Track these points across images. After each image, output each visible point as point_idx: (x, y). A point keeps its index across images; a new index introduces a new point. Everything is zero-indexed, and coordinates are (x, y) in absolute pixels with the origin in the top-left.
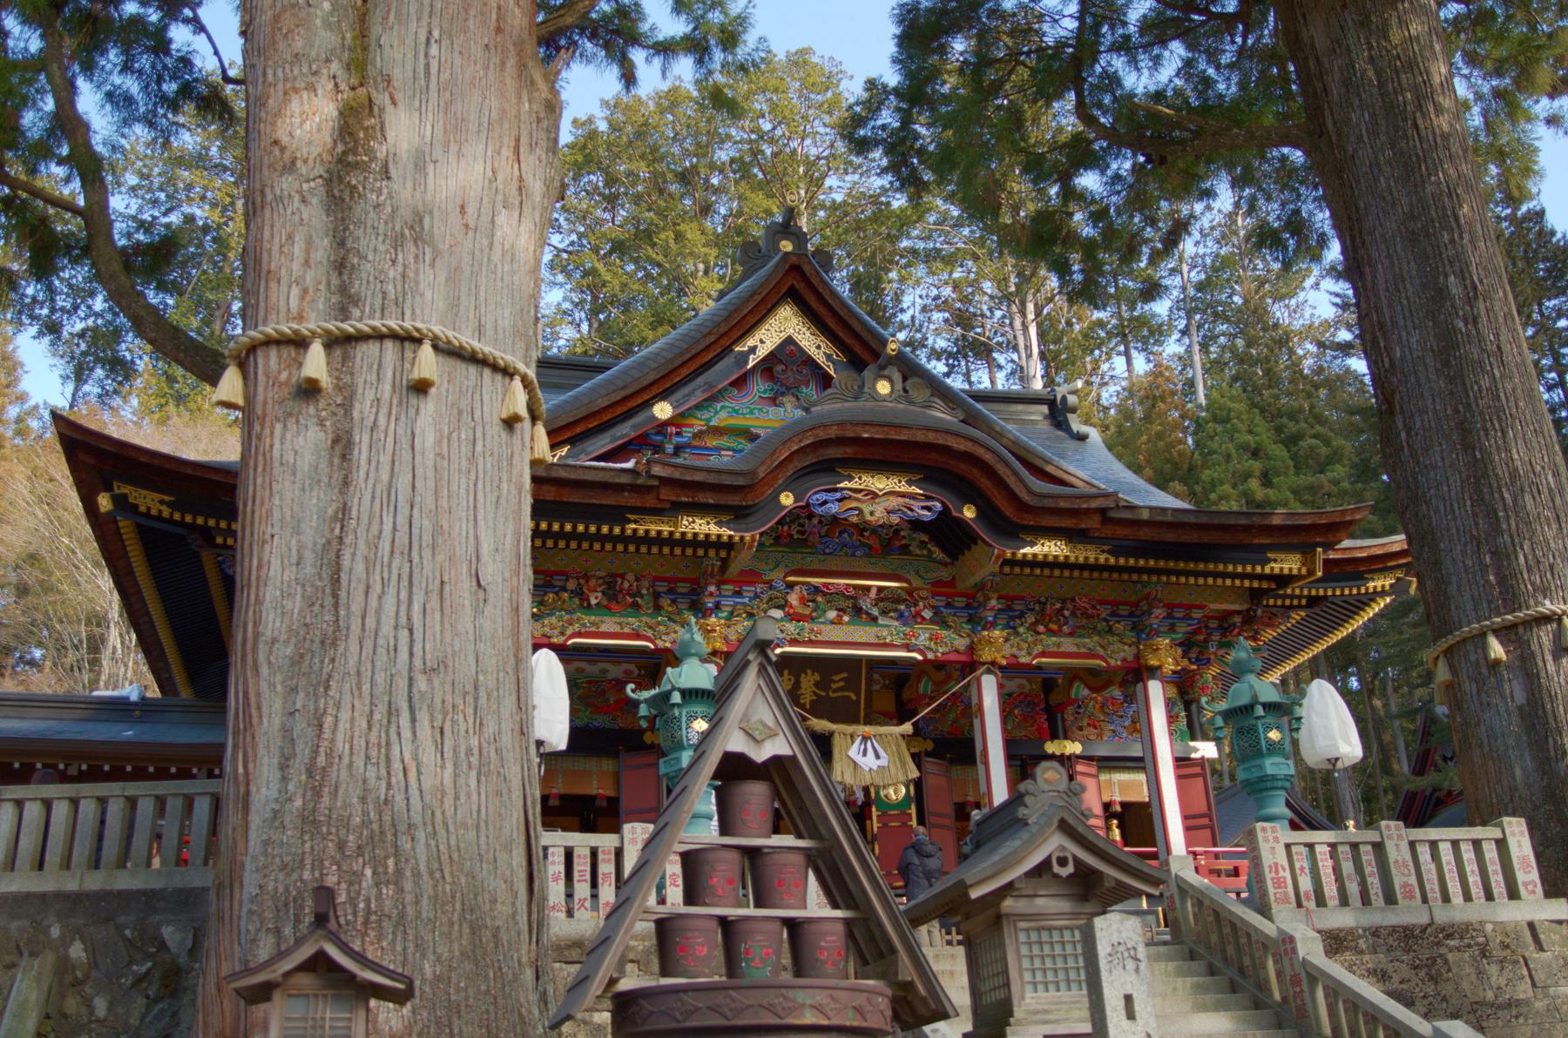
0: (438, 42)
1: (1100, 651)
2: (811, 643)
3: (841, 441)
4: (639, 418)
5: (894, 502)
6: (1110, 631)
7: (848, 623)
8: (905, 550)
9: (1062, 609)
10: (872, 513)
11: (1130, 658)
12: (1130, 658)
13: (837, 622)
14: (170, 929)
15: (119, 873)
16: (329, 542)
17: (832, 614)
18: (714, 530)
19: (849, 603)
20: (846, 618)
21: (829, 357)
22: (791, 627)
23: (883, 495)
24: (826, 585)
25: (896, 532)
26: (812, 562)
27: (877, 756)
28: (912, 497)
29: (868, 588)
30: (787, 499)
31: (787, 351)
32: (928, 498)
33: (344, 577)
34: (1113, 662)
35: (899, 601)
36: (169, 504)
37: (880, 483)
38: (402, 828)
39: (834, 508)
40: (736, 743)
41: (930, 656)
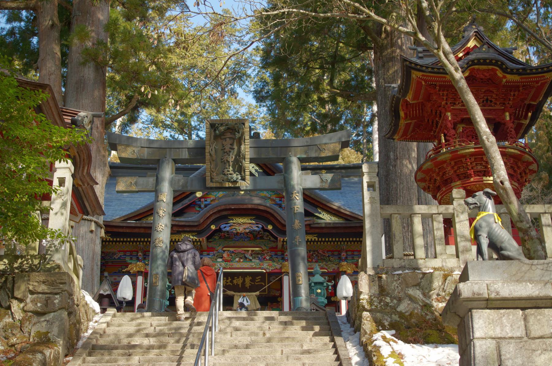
2: (230, 268)
3: (226, 210)
4: (191, 197)
6: (329, 260)
8: (262, 238)
11: (336, 269)
12: (336, 269)
13: (239, 261)
17: (237, 259)
19: (243, 255)
20: (242, 260)
21: (256, 171)
22: (223, 264)
24: (235, 250)
25: (259, 232)
26: (231, 243)
27: (247, 302)
29: (248, 251)
30: (213, 227)
34: (330, 270)
35: (258, 254)
37: (241, 220)
39: (227, 229)
40: (102, 292)
41: (268, 271)
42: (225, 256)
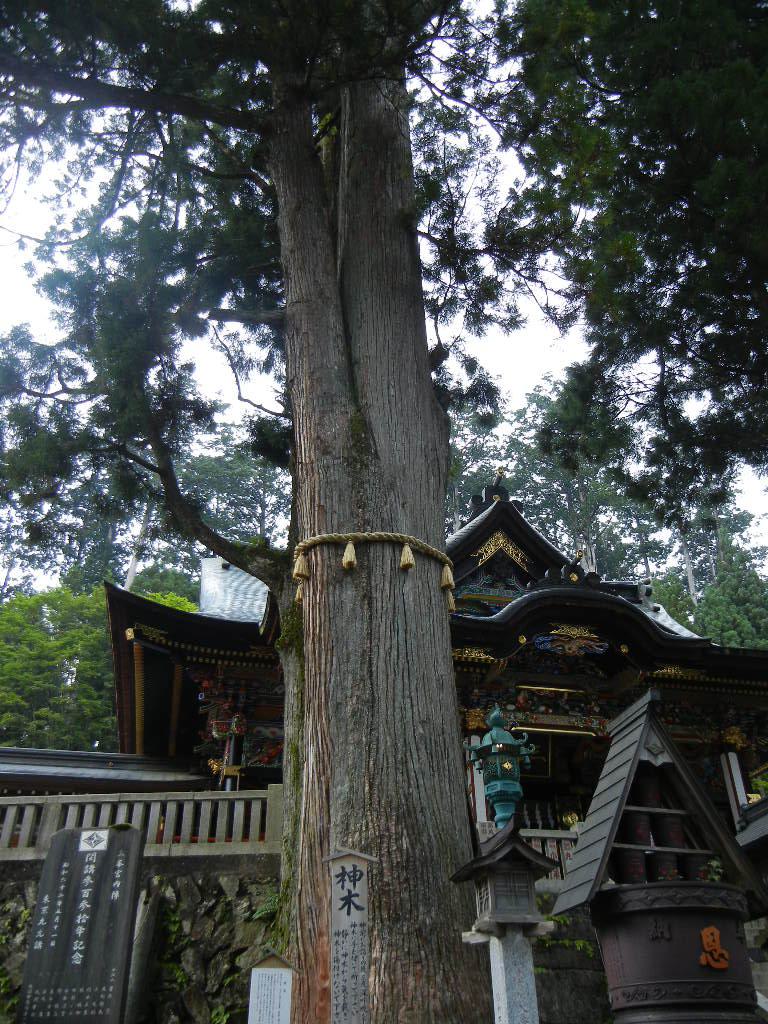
0: (394, 387)
1: (698, 733)
5: (583, 643)
7: (552, 714)
9: (674, 708)
10: (570, 649)
13: (546, 713)
14: (226, 879)
15: (193, 845)
16: (364, 651)
18: (483, 657)
22: (520, 715)
23: (575, 638)
28: (592, 640)
31: (500, 555)
32: (601, 641)
33: (374, 669)
36: (166, 636)
37: (575, 632)
38: (419, 809)
42: (522, 701)
